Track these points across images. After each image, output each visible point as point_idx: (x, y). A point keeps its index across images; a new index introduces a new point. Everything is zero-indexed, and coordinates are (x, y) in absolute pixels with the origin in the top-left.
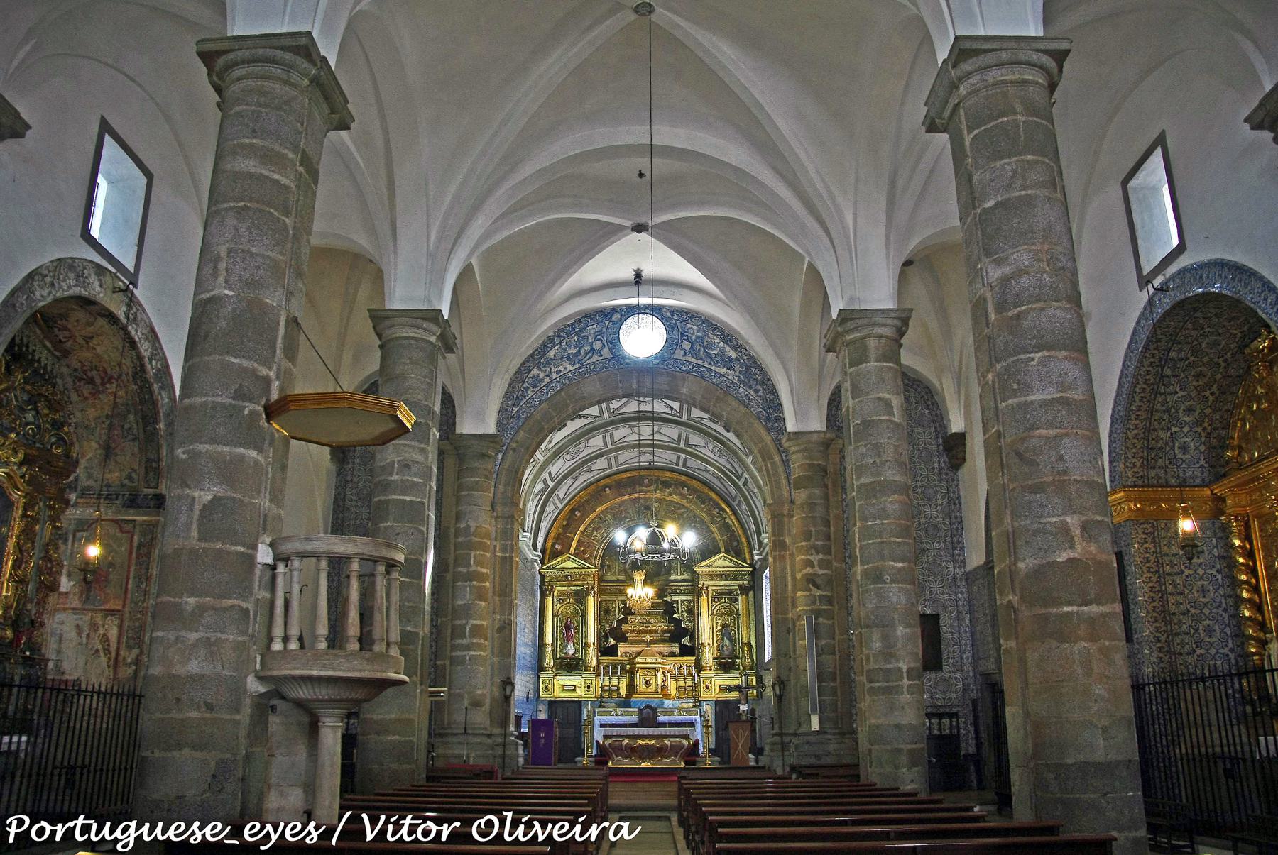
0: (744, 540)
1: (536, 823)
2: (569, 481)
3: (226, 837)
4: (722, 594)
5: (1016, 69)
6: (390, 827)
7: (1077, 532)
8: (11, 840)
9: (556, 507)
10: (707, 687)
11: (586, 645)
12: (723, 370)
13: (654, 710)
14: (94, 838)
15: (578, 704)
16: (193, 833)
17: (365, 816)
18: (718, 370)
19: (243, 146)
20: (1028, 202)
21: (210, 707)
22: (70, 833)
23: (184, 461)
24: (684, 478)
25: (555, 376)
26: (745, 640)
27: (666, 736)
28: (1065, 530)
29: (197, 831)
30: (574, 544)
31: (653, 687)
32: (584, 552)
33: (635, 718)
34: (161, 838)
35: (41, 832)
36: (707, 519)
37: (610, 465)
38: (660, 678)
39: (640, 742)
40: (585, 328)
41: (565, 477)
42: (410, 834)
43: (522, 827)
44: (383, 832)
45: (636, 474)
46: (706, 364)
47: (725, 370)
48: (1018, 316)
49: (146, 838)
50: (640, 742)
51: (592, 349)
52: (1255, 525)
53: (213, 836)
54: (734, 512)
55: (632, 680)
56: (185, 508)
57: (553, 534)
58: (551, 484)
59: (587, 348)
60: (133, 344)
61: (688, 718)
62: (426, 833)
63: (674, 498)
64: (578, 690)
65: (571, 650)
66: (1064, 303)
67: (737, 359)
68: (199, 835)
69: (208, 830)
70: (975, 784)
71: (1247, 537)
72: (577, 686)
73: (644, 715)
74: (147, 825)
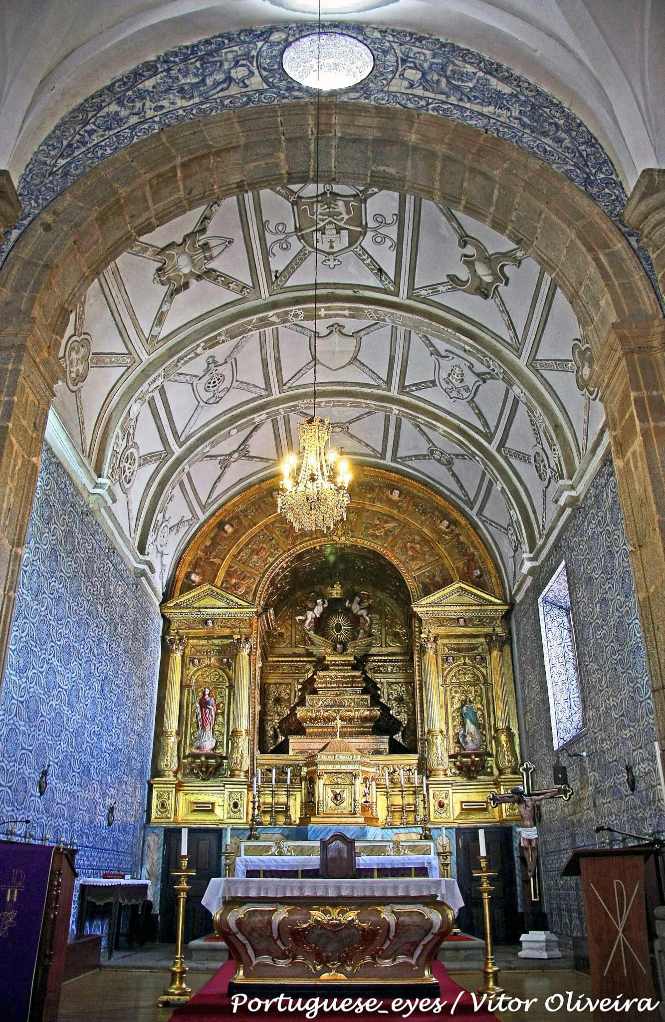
1: (588, 999)
3: (380, 1009)
4: (459, 650)
6: (490, 1002)
8: (235, 1011)
10: (441, 805)
11: (233, 735)
13: (350, 843)
14: (291, 1010)
15: (218, 833)
16: (357, 1006)
17: (473, 994)
22: (274, 1006)
26: (501, 725)
27: (385, 901)
29: (360, 1004)
31: (346, 805)
32: (236, 586)
33: (314, 861)
34: (336, 1009)
35: (255, 1005)
38: (359, 788)
39: (317, 915)
42: (503, 1007)
43: (579, 1002)
44: (485, 1005)
49: (326, 1009)
50: (317, 915)
51: (229, 79)
53: (371, 1008)
55: (311, 793)
57: (189, 558)
59: (220, 77)
61: (412, 859)
62: (515, 1005)
64: (218, 810)
65: (208, 744)
68: (361, 1007)
69: (367, 1004)
72: (222, 805)
73: (331, 854)
74: (326, 1001)
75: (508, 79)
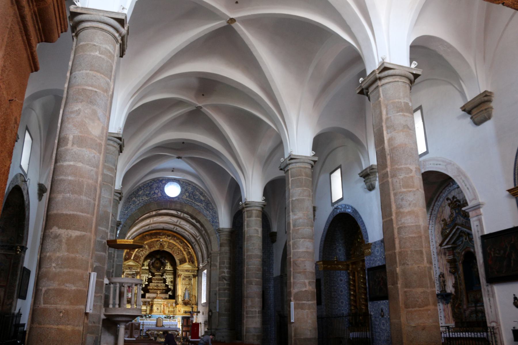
0: (195, 258)
5: (304, 164)
7: (307, 284)
12: (199, 204)
20: (303, 200)
21: (94, 323)
24: (175, 234)
25: (141, 201)
26: (194, 294)
28: (305, 283)
30: (133, 256)
31: (159, 311)
36: (182, 250)
45: (158, 231)
48: (298, 229)
51: (155, 193)
52: (356, 273)
54: (193, 248)
59: (153, 192)
63: (171, 241)
66: (309, 227)
70: (481, 308)
71: (354, 276)
75: (204, 196)
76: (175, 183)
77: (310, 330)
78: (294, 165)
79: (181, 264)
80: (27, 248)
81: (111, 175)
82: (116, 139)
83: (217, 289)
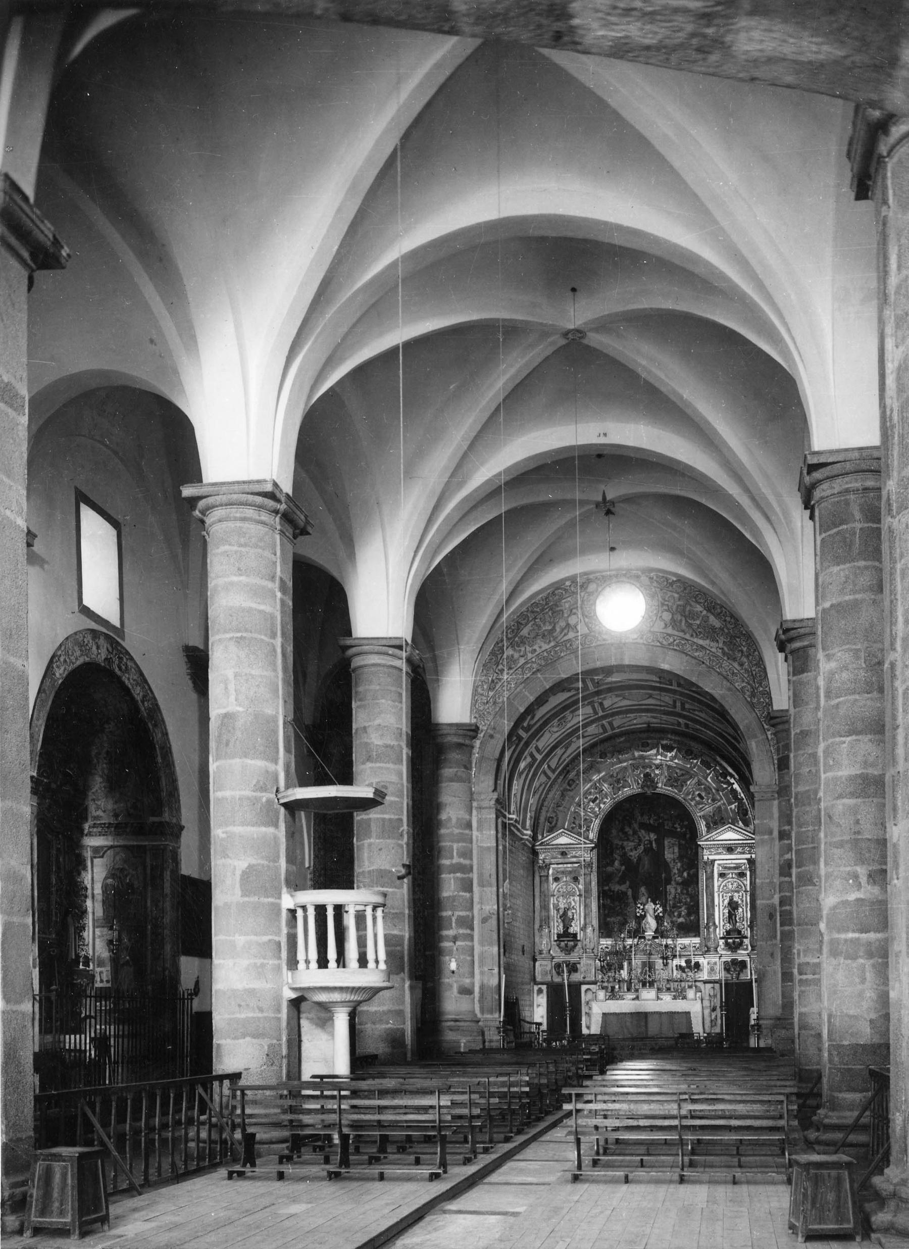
2: (559, 751)
7: (863, 879)
9: (549, 778)
18: (701, 642)
19: (232, 584)
23: (223, 839)
37: (605, 731)
40: (560, 600)
41: (554, 748)
46: (687, 636)
47: (708, 642)
51: (568, 625)
56: (229, 874)
58: (539, 757)
59: (562, 624)
60: (127, 691)
67: (721, 629)
76: (628, 586)
77: (871, 1021)
78: (825, 486)
79: (709, 829)
80: (182, 828)
81: (262, 607)
82: (259, 500)
83: (776, 900)
